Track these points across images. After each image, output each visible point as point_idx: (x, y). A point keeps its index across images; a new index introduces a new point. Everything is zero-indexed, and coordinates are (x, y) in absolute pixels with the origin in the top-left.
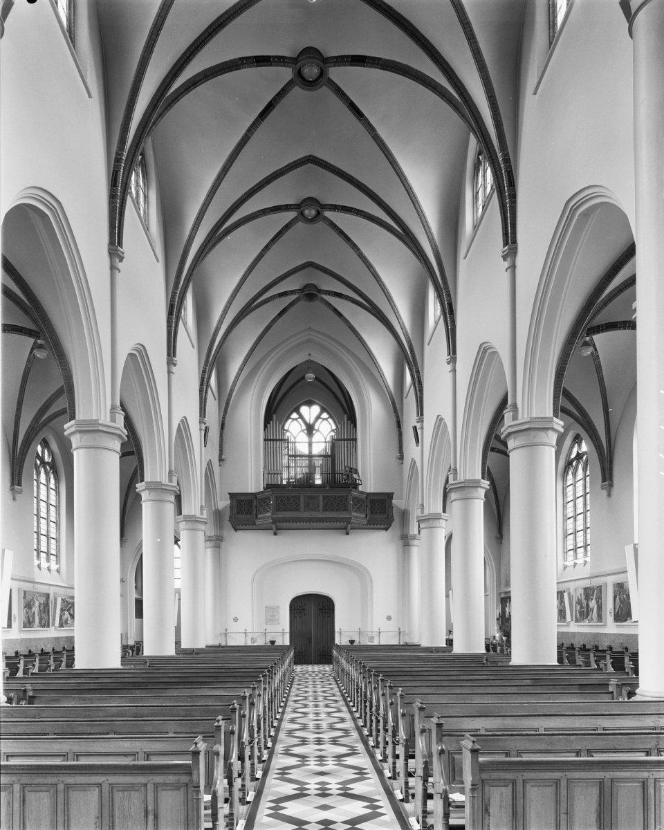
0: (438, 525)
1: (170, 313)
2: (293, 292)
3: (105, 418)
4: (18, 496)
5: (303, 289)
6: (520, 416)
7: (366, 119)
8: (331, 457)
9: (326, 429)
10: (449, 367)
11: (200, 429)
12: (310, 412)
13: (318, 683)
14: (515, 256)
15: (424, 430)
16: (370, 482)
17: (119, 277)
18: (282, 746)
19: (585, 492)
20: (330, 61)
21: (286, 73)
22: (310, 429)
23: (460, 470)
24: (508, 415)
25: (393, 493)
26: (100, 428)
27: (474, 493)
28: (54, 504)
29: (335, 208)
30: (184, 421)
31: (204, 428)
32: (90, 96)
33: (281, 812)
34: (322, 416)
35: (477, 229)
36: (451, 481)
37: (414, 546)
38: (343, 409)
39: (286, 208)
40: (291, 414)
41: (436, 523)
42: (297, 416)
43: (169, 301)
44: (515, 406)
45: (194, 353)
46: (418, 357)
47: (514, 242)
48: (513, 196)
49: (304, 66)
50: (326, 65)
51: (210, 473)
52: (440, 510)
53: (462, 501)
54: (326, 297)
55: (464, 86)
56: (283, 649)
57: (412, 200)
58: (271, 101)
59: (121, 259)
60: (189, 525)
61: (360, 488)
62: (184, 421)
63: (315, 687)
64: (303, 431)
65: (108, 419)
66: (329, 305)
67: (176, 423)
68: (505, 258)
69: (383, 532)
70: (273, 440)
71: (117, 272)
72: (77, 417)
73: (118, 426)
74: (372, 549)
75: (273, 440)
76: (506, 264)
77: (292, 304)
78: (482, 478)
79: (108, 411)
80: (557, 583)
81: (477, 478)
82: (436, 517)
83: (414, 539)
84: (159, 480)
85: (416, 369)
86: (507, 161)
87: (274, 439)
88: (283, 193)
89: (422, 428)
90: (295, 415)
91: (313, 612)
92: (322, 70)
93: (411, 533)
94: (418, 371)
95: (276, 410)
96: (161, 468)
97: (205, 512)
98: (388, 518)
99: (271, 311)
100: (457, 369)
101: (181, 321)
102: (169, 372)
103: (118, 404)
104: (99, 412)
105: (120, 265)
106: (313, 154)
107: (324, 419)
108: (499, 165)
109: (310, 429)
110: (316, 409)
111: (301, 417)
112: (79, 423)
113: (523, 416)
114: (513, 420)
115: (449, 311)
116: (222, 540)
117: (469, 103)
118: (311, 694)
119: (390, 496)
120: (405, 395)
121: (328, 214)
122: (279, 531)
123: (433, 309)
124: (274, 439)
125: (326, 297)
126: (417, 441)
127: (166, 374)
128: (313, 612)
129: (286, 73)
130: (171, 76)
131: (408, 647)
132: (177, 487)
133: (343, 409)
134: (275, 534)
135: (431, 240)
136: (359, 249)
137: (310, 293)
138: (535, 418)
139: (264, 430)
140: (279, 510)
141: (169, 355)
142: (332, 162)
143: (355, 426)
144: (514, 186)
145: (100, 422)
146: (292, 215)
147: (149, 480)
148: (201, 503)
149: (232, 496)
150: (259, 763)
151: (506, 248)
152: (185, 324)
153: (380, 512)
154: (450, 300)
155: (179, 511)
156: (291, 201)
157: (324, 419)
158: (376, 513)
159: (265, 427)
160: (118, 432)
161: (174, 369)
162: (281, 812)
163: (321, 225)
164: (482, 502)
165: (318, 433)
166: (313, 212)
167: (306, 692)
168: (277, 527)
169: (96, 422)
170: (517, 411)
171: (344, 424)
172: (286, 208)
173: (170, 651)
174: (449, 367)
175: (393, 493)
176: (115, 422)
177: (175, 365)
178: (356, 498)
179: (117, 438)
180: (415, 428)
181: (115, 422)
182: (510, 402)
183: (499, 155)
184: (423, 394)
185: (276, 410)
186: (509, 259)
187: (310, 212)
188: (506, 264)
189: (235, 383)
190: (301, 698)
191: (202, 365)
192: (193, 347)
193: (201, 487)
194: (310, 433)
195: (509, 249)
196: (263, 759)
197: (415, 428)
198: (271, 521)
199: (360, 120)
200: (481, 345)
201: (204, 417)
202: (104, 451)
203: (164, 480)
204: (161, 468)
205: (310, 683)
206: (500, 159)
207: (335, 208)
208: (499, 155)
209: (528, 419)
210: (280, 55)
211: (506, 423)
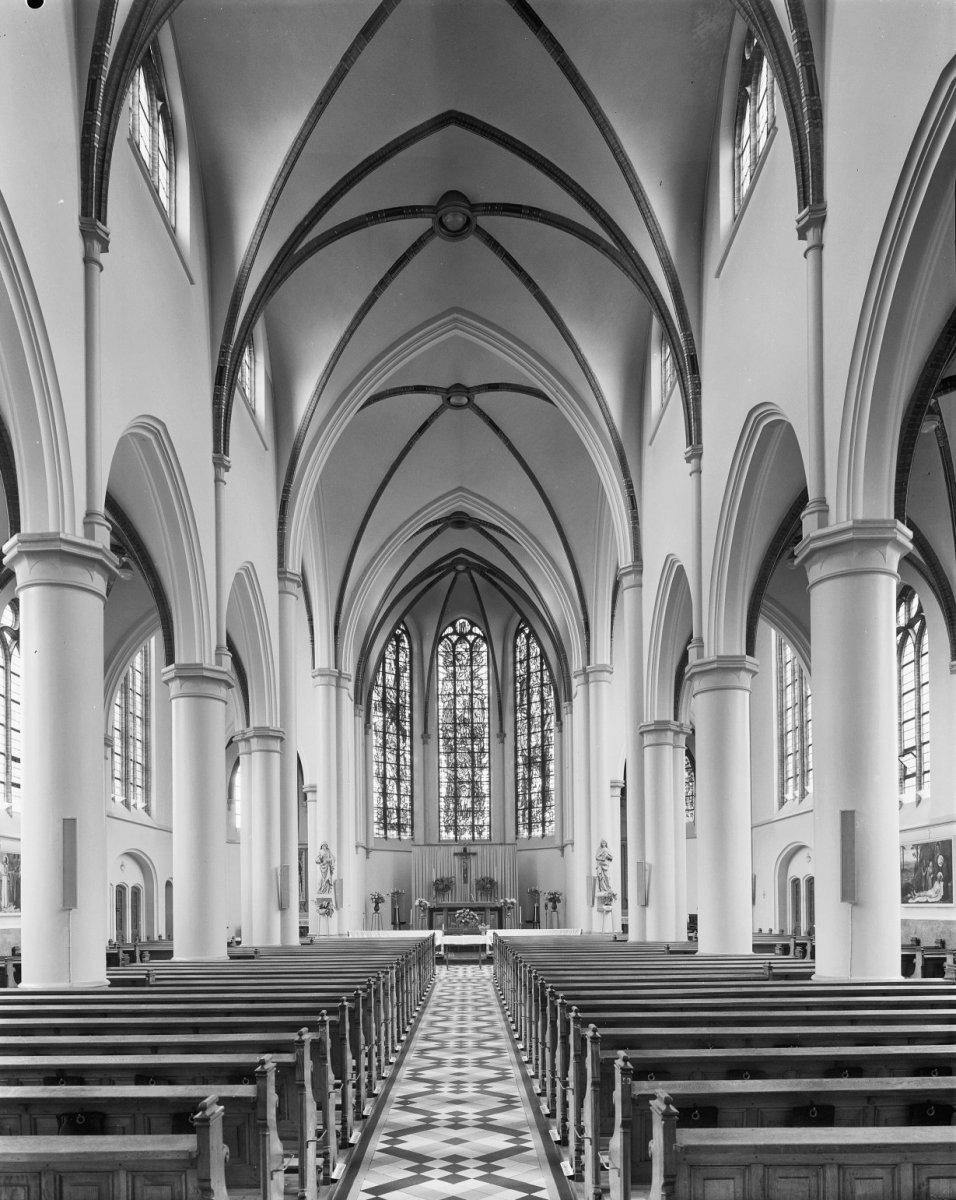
0: (882, 566)
1: (219, 380)
3: (209, 661)
13: (470, 1033)
14: (700, 460)
19: (919, 682)
20: (478, 209)
21: (435, 401)
23: (709, 643)
24: (809, 524)
26: (206, 674)
27: (874, 559)
28: (119, 753)
29: (494, 209)
32: (192, 283)
33: (414, 1164)
35: (740, 221)
36: (693, 658)
39: (412, 211)
41: (732, 679)
43: (280, 497)
44: (700, 640)
47: (820, 197)
49: (446, 215)
50: (475, 213)
52: (740, 649)
57: (627, 179)
59: (227, 469)
60: (189, 687)
63: (463, 994)
65: (214, 663)
68: (688, 460)
71: (222, 484)
72: (23, 531)
73: (99, 546)
76: (690, 467)
77: (438, 532)
79: (213, 653)
80: (901, 831)
81: (738, 653)
82: (727, 667)
84: (198, 661)
88: (409, 181)
92: (468, 218)
96: (202, 642)
100: (827, 241)
101: (237, 391)
102: (218, 480)
103: (100, 506)
104: (202, 652)
112: (179, 668)
113: (709, 654)
114: (819, 528)
115: (689, 368)
118: (454, 1033)
120: (647, 436)
121: (484, 221)
123: (660, 367)
127: (81, 266)
131: (644, 943)
135: (660, 248)
137: (456, 216)
138: (863, 522)
141: (216, 450)
145: (204, 666)
146: (423, 224)
147: (183, 661)
151: (803, 212)
154: (694, 349)
155: (170, 658)
156: (423, 198)
160: (99, 556)
161: (226, 476)
162: (414, 1164)
163: (472, 242)
166: (461, 220)
167: (451, 1000)
169: (199, 667)
170: (827, 511)
172: (412, 211)
173: (220, 954)
176: (93, 539)
177: (227, 469)
179: (223, 684)
181: (93, 539)
186: (693, 461)
187: (454, 220)
189: (309, 419)
190: (439, 1024)
199: (536, 32)
200: (668, 557)
202: (213, 701)
203: (207, 661)
204: (202, 642)
205: (456, 1010)
207: (494, 209)
208: (681, 335)
209: (715, 658)
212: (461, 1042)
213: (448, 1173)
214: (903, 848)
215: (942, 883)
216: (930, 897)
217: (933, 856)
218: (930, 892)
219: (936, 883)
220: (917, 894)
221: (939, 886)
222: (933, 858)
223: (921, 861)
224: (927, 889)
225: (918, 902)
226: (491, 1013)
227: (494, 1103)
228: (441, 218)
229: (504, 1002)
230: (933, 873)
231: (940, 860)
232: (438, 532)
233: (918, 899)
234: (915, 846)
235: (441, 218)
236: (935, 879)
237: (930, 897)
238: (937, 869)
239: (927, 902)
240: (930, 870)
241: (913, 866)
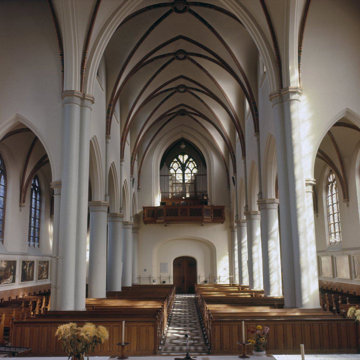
2: (169, 54)
4: (22, 209)
5: (179, 111)
7: (204, 69)
8: (194, 183)
9: (192, 168)
11: (131, 180)
12: (183, 158)
16: (214, 200)
17: (109, 146)
18: (168, 339)
22: (183, 167)
25: (225, 206)
29: (196, 4)
30: (113, 164)
31: (132, 179)
34: (190, 160)
37: (244, 226)
38: (201, 162)
40: (174, 159)
42: (176, 160)
45: (129, 147)
46: (254, 95)
51: (126, 188)
54: (191, 57)
56: (170, 287)
61: (209, 204)
62: (113, 164)
64: (179, 167)
66: (193, 94)
67: (109, 165)
69: (222, 224)
70: (164, 176)
74: (216, 234)
75: (164, 176)
77: (172, 94)
79: (104, 196)
83: (257, 214)
85: (241, 130)
87: (165, 175)
89: (236, 178)
90: (175, 160)
91: (185, 267)
93: (253, 210)
94: (233, 153)
95: (166, 161)
97: (132, 219)
98: (222, 219)
99: (154, 67)
107: (191, 162)
109: (183, 167)
110: (186, 157)
111: (179, 160)
116: (138, 229)
119: (223, 208)
120: (246, 118)
122: (168, 224)
124: (165, 175)
125: (191, 57)
126: (234, 185)
127: (105, 144)
128: (185, 267)
130: (130, 74)
133: (201, 162)
134: (166, 226)
136: (204, 102)
139: (160, 171)
140: (168, 216)
142: (190, 78)
143: (206, 168)
148: (131, 215)
149: (144, 208)
153: (219, 215)
157: (191, 162)
158: (217, 216)
159: (161, 169)
161: (123, 163)
165: (187, 169)
168: (167, 222)
171: (201, 167)
175: (225, 206)
178: (206, 209)
180: (233, 178)
185: (166, 161)
187: (181, 56)
191: (109, 101)
192: (129, 145)
193: (106, 182)
194: (184, 172)
196: (163, 338)
197: (233, 178)
198: (164, 221)
201: (133, 174)
207: (196, 4)
210: (169, 52)
212: (185, 321)
213: (182, 348)
214: (1, 261)
215: (12, 276)
216: (9, 281)
217: (11, 265)
218: (9, 279)
219: (11, 276)
220: (5, 280)
221: (11, 277)
222: (10, 267)
223: (7, 267)
224: (8, 278)
225: (5, 284)
226: (193, 305)
227: (195, 334)
228: (77, 339)
229: (200, 315)
230: (10, 272)
231: (13, 268)
232: (172, 94)
233: (5, 282)
234: (5, 261)
235: (77, 339)
236: (10, 274)
237: (9, 281)
238: (11, 270)
239: (8, 283)
240: (9, 271)
241: (4, 269)
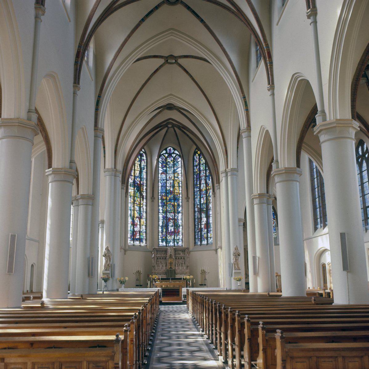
6: (328, 119)
10: (270, 93)
14: (316, 16)
15: (318, 24)
44: (277, 161)
48: (271, 63)
53: (286, 182)
55: (246, 15)
58: (152, 9)
68: (309, 17)
78: (297, 167)
86: (267, 45)
105: (42, 17)
106: (173, 54)
108: (264, 49)
113: (330, 118)
117: (248, 21)
127: (72, 94)
129: (162, 61)
132: (76, 172)
144: (271, 58)
147: (6, 117)
150: (144, 357)
151: (309, 10)
152: (87, 62)
164: (354, 142)
174: (270, 93)
182: (275, 159)
183: (264, 44)
184: (272, 65)
186: (312, 18)
188: (310, 21)
195: (311, 11)
206: (264, 46)
211: (273, 170)
